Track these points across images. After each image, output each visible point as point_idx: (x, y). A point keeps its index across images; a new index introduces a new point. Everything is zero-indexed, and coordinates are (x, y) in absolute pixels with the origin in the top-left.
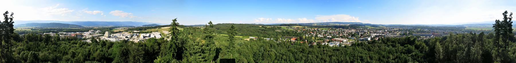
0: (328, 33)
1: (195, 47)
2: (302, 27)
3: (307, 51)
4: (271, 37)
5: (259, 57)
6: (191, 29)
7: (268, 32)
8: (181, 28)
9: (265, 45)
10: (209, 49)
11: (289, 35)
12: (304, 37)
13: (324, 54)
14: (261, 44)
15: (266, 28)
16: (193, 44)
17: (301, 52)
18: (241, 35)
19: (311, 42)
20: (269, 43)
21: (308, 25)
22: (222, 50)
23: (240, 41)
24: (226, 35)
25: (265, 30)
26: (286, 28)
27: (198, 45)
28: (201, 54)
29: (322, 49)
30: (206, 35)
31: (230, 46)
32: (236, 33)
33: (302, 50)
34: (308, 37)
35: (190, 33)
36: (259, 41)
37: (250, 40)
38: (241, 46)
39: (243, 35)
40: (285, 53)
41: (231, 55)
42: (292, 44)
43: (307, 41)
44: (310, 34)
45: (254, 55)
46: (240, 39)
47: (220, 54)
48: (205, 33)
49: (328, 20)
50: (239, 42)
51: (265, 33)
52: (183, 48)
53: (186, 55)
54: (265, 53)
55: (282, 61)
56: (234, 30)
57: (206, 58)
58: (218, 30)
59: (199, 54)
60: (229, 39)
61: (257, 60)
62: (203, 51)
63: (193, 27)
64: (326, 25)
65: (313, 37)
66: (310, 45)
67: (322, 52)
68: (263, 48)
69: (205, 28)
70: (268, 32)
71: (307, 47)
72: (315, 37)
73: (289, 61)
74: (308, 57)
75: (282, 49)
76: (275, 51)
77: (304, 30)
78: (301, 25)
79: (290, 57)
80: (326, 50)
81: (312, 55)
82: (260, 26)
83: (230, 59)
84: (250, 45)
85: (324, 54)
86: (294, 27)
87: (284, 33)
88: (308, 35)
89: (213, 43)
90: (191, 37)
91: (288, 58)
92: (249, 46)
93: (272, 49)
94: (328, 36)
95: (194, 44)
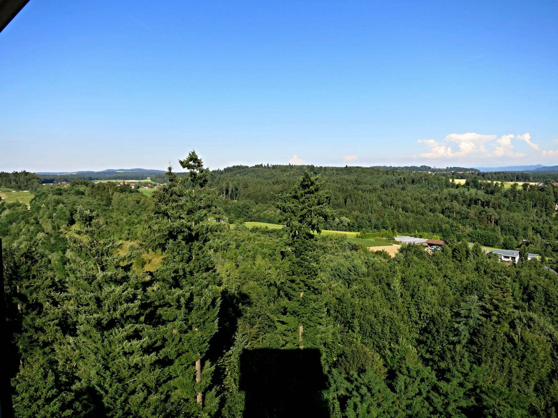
1: (107, 289)
5: (453, 343)
6: (83, 194)
7: (504, 214)
8: (19, 188)
10: (183, 300)
14: (464, 277)
16: (94, 277)
18: (350, 228)
22: (250, 304)
23: (347, 257)
24: (271, 226)
25: (485, 204)
27: (126, 279)
28: (137, 326)
30: (167, 224)
31: (293, 281)
32: (326, 217)
35: (77, 216)
37: (401, 251)
38: (349, 283)
39: (359, 228)
41: (301, 329)
45: (425, 330)
46: (343, 248)
47: (240, 322)
48: (165, 214)
50: (342, 261)
52: (15, 300)
53: (42, 338)
54: (489, 329)
56: (313, 199)
57: (169, 351)
58: (232, 198)
59: (129, 328)
60: (289, 249)
61: (443, 358)
62: (153, 313)
63: (97, 182)
68: (481, 299)
69: (165, 190)
82: (457, 181)
83: (297, 352)
84: (403, 280)
89: (207, 269)
90: (85, 239)
92: (396, 283)
93: (535, 316)
95: (100, 275)
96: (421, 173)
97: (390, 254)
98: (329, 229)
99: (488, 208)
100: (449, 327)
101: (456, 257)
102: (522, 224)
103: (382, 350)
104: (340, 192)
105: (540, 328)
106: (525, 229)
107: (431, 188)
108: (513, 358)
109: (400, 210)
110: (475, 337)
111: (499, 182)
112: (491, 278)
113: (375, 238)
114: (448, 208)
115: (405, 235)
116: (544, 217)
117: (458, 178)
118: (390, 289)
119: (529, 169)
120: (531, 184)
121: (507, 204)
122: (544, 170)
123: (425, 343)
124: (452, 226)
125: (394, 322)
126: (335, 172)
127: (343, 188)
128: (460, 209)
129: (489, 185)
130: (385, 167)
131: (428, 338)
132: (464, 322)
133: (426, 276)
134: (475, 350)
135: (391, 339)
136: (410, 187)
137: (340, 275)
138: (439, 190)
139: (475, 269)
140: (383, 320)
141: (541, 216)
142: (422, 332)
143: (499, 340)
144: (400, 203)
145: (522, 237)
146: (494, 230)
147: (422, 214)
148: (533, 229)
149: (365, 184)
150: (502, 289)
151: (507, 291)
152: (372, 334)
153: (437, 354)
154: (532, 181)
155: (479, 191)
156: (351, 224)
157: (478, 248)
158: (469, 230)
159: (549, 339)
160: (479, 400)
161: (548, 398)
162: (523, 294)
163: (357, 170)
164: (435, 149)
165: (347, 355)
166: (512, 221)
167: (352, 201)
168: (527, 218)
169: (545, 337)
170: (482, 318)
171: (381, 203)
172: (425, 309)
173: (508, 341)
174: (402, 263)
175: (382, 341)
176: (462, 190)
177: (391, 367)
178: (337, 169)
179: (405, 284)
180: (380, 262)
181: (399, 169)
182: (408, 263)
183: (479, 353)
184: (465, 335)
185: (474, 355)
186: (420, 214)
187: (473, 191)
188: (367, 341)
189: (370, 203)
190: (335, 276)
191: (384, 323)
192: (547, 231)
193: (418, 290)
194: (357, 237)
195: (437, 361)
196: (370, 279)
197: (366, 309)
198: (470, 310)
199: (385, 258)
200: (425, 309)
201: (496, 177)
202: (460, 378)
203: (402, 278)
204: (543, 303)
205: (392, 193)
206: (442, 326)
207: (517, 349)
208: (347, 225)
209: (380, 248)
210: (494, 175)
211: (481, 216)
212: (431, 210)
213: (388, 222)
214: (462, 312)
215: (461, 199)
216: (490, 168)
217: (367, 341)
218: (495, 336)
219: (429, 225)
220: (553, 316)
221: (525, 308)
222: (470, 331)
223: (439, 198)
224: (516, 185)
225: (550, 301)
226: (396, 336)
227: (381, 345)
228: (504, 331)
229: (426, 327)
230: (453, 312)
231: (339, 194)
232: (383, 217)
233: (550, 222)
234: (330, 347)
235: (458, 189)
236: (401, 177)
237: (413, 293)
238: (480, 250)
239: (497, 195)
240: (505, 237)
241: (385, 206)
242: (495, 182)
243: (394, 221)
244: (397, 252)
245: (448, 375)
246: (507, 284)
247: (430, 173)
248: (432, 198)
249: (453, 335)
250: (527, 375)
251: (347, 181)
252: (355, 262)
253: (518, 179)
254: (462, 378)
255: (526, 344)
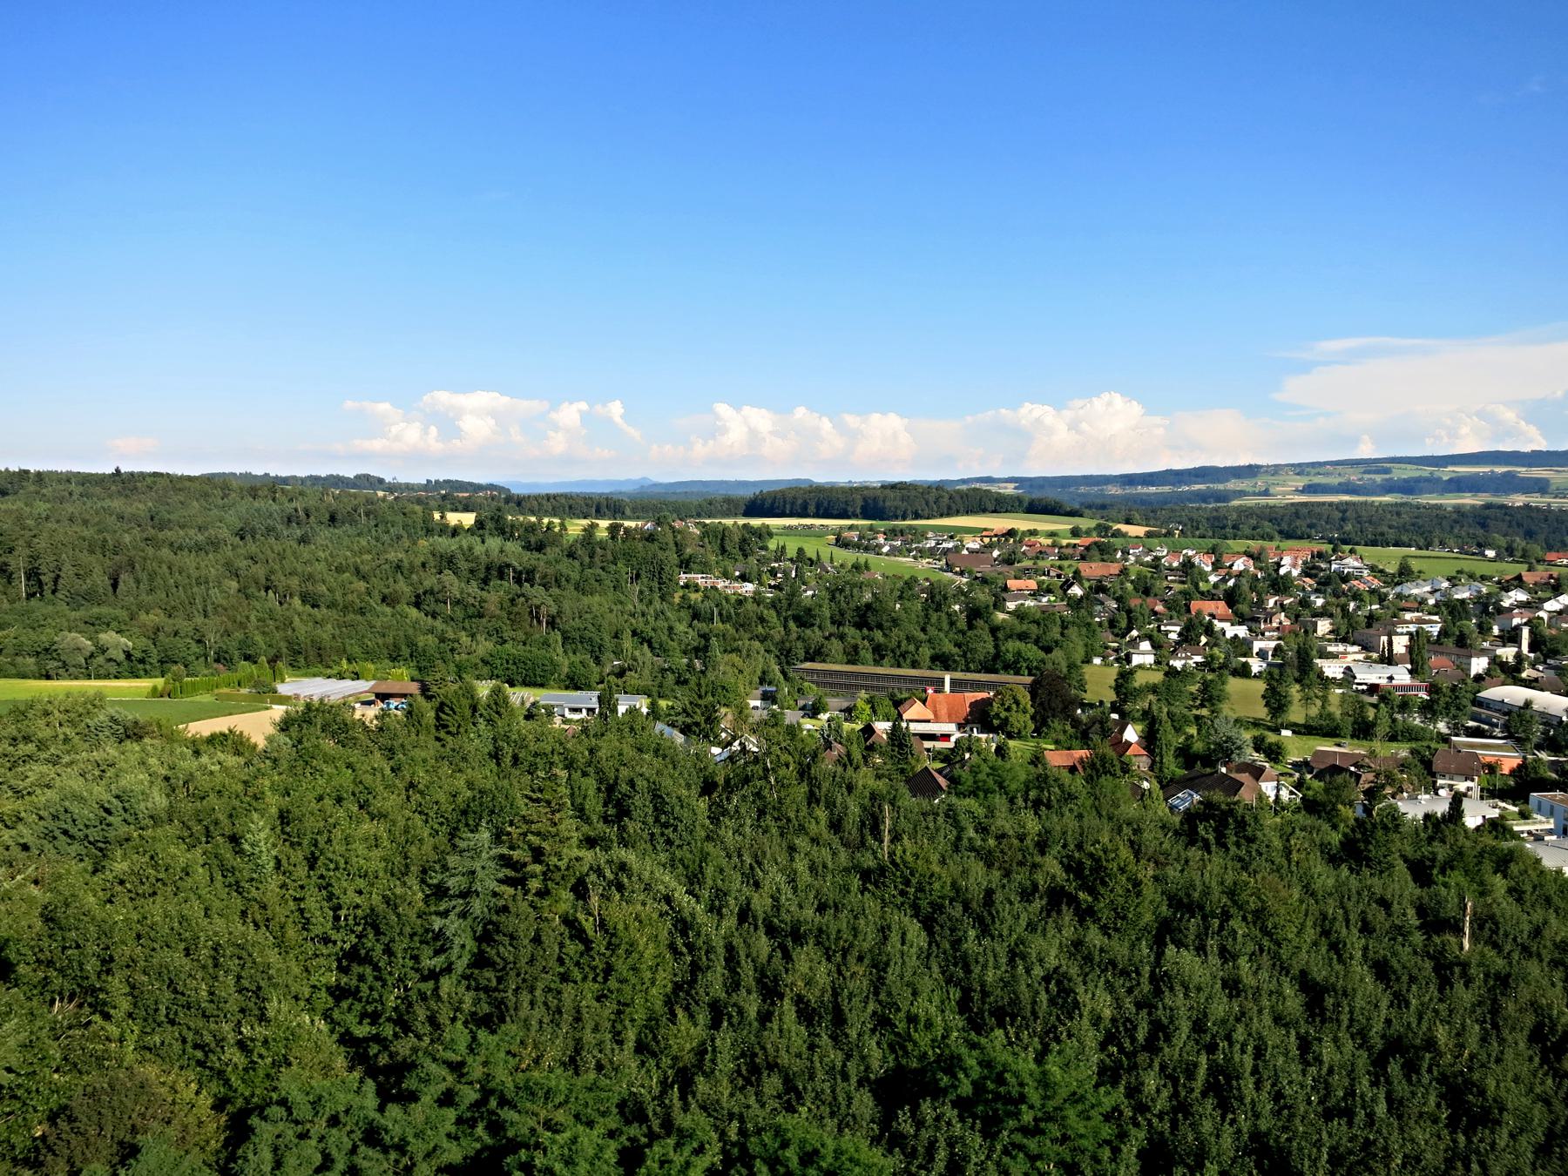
0: (1511, 637)
2: (1062, 525)
3: (1150, 891)
4: (621, 673)
5: (433, 975)
7: (571, 602)
9: (518, 787)
11: (879, 653)
12: (1099, 680)
13: (1444, 983)
15: (538, 543)
17: (1057, 898)
18: (133, 665)
19: (1209, 760)
20: (582, 757)
21: (1164, 500)
23: (103, 768)
25: (525, 576)
26: (842, 543)
29: (1402, 886)
33: (1072, 867)
34: (1157, 677)
36: (427, 739)
37: (285, 725)
38: (100, 853)
40: (822, 908)
42: (922, 784)
43: (1150, 740)
44: (1187, 638)
45: (352, 956)
49: (1509, 416)
51: (520, 614)
55: (771, 1037)
64: (1468, 500)
65: (1234, 684)
66: (1187, 799)
67: (1400, 931)
68: (498, 837)
70: (571, 602)
71: (1150, 837)
72: (1274, 677)
73: (882, 1022)
74: (1161, 981)
75: (773, 846)
76: (669, 881)
77: (1093, 569)
78: (1051, 495)
79: (892, 975)
80: (1487, 925)
81: (1226, 954)
82: (453, 518)
85: (1444, 983)
86: (953, 533)
87: (804, 618)
88: (1156, 646)
91: (859, 979)
92: (260, 834)
93: (630, 857)
94: (1514, 694)
96: (355, 496)
97: (253, 740)
98: (58, 677)
99: (532, 586)
100: (420, 931)
101: (445, 726)
102: (610, 624)
103: (211, 1055)
104: (92, 552)
105: (643, 886)
106: (616, 636)
107: (386, 538)
108: (585, 978)
109: (297, 602)
110: (489, 945)
111: (557, 521)
112: (529, 773)
113: (216, 691)
114: (431, 592)
115: (315, 675)
116: (657, 604)
117: (456, 510)
118: (239, 852)
119: (624, 489)
120: (627, 523)
121: (575, 576)
122: (656, 490)
123: (354, 993)
124: (442, 640)
125: (250, 955)
126: (77, 490)
127: (105, 540)
128: (462, 593)
129: (531, 528)
130: (248, 476)
131: (361, 978)
132: (458, 910)
133: (354, 794)
134: (489, 980)
135: (242, 1011)
136: (324, 535)
137: (73, 831)
138: (406, 543)
139: (489, 754)
140: (214, 958)
141: (651, 602)
142: (345, 963)
143: (550, 939)
144: (294, 582)
145: (612, 656)
146: (546, 644)
147: (362, 612)
148: (634, 633)
149: (182, 527)
150: (548, 803)
151: (561, 806)
152: (176, 1013)
153: (389, 1019)
154: (629, 518)
155: (509, 544)
156: (138, 654)
157: (501, 696)
158: (484, 646)
159: (666, 908)
160: (496, 1127)
161: (666, 1061)
162: (605, 805)
163: (155, 483)
164: (394, 430)
165: (76, 1113)
166: (588, 616)
167: (138, 581)
168: (620, 607)
169: (655, 905)
170: (504, 888)
171: (234, 584)
172: (350, 893)
173: (571, 938)
174: (284, 765)
175: (213, 1026)
176: (465, 541)
177: (245, 1099)
178: (86, 480)
179: (288, 829)
180: (218, 767)
181: (291, 481)
182: (304, 758)
183: (501, 987)
184: (463, 946)
185: (489, 996)
186: (354, 612)
187: (494, 543)
188: (157, 1039)
189: (199, 584)
190: (55, 838)
191: (216, 966)
192: (665, 638)
193: (329, 841)
194: (154, 692)
195: (390, 1038)
196: (172, 830)
197: (152, 934)
198: (473, 873)
199: (238, 753)
200: (350, 893)
201: (548, 506)
202: (444, 1079)
203: (281, 811)
204: (650, 820)
205: (269, 552)
206: (401, 933)
207: (592, 953)
208: (122, 657)
209: (219, 725)
210: (544, 502)
211: (516, 609)
212: (384, 600)
213: (259, 638)
214: (451, 883)
215: (463, 565)
216: (536, 485)
217: (157, 1039)
218: (538, 931)
219: (380, 641)
220: (674, 848)
221: (612, 841)
222: (475, 932)
223: (406, 564)
224: (593, 526)
225: (665, 813)
226: (258, 998)
227: (208, 1038)
228: (560, 911)
229: (354, 947)
230: (429, 886)
231: (92, 558)
232: (242, 626)
233: (669, 614)
234: (19, 1093)
235: (457, 539)
236: (298, 504)
237: (313, 853)
238: (506, 700)
239: (551, 553)
240: (573, 658)
241: (249, 591)
242: (546, 521)
243: (278, 635)
244: (271, 730)
245: (410, 1083)
246: (559, 789)
247: (381, 494)
248: (387, 566)
249: (431, 953)
250: (619, 1013)
251: (121, 517)
252: (126, 781)
253: (599, 514)
254: (450, 1078)
255: (613, 935)
